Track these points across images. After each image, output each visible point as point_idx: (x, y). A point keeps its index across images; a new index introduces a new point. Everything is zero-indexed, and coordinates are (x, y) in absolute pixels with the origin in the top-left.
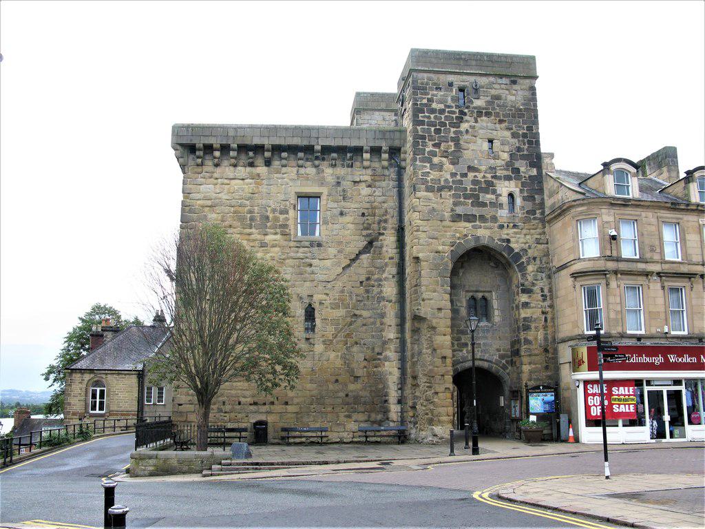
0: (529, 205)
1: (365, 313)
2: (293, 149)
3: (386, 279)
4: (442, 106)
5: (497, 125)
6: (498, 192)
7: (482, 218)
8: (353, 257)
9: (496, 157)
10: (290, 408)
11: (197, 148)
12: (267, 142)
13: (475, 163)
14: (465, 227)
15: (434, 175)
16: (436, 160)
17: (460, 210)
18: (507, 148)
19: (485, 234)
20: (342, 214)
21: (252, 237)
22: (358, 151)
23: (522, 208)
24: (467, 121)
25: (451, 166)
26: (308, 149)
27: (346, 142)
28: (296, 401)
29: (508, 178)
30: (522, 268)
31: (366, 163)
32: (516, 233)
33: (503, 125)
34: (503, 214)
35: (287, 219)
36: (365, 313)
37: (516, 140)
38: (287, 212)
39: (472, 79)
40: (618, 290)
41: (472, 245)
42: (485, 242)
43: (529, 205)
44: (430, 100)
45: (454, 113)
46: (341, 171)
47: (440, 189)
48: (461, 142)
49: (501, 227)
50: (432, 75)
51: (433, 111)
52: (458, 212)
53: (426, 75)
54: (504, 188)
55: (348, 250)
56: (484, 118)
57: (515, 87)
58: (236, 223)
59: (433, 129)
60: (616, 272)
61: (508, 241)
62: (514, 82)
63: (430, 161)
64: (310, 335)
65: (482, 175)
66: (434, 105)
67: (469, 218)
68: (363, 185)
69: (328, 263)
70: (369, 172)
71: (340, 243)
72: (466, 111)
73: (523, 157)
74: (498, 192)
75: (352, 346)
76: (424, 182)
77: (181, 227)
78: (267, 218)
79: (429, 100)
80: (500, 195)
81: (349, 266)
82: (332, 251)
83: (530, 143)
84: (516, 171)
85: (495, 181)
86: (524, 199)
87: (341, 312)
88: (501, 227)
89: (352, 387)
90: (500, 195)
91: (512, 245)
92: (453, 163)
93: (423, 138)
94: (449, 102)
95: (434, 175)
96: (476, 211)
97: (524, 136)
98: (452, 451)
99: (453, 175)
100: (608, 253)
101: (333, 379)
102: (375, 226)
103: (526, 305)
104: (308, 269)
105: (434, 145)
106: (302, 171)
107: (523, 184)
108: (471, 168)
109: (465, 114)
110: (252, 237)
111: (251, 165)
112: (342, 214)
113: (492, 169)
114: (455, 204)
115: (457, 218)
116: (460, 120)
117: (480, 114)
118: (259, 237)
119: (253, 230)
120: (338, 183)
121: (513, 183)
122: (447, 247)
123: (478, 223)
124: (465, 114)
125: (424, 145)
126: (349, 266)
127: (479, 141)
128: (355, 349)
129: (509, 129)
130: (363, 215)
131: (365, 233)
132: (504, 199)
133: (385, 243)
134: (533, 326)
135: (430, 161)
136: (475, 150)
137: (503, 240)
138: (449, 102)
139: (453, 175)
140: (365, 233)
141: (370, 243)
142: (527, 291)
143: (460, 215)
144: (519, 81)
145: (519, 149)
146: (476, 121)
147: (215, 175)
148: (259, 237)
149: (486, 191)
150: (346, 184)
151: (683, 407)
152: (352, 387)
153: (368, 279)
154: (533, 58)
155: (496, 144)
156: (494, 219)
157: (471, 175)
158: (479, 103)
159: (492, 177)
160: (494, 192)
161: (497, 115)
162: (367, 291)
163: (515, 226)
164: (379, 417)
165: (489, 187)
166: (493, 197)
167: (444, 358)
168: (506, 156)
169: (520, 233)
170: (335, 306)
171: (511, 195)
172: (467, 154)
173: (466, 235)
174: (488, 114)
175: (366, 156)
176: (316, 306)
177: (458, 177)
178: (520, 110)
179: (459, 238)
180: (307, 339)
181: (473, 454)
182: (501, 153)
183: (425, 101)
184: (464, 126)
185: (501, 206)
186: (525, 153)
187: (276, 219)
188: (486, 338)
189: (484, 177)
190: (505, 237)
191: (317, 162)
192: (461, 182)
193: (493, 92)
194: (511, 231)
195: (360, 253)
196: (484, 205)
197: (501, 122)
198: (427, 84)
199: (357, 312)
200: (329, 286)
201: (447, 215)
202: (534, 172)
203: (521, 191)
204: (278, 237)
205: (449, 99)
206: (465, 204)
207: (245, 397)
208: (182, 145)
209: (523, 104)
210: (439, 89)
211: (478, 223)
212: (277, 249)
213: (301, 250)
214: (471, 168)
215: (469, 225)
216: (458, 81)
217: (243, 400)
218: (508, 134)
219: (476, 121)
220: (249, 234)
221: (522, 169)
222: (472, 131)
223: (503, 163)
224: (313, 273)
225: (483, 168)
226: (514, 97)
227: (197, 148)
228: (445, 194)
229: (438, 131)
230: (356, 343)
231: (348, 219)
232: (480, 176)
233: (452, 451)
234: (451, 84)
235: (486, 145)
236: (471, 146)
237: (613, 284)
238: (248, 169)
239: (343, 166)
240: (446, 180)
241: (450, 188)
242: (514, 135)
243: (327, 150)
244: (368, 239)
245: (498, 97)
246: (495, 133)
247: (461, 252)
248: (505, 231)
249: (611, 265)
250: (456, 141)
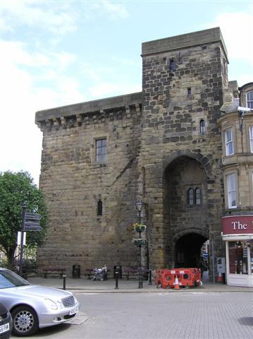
0: (214, 126)
1: (128, 203)
2: (90, 115)
3: (139, 182)
4: (159, 73)
5: (194, 78)
6: (193, 120)
7: (183, 138)
8: (122, 170)
9: (192, 98)
10: (90, 258)
11: (47, 120)
12: (77, 113)
13: (179, 105)
14: (171, 146)
15: (154, 116)
16: (155, 107)
17: (169, 135)
18: (199, 91)
19: (184, 148)
20: (116, 147)
21: (73, 165)
22: (123, 109)
23: (209, 128)
24: (174, 79)
25: (165, 109)
26: (97, 113)
27: (118, 106)
28: (92, 254)
29: (200, 110)
30: (209, 167)
31: (129, 116)
32: (204, 145)
33: (197, 77)
34: (196, 134)
35: (89, 153)
36: (128, 203)
37: (205, 85)
38: (89, 150)
39: (178, 52)
40: (247, 176)
41: (176, 156)
42: (184, 153)
43: (214, 126)
44: (152, 72)
45: (167, 76)
46: (116, 122)
47: (157, 124)
48: (170, 93)
49: (195, 142)
50: (154, 56)
51: (154, 78)
52: (168, 137)
53: (150, 57)
54: (196, 118)
55: (119, 167)
56: (185, 75)
57: (205, 51)
58: (65, 159)
59: (154, 88)
60: (244, 164)
61: (199, 150)
62: (205, 48)
63: (151, 108)
64: (100, 217)
65: (182, 111)
66: (155, 74)
67: (174, 139)
68: (128, 128)
69: (109, 176)
70: (131, 120)
71: (115, 163)
72: (174, 73)
73: (210, 95)
74: (193, 120)
75: (121, 222)
76: (148, 121)
77: (42, 164)
78: (80, 154)
79: (152, 72)
80: (194, 122)
81: (120, 176)
82: (111, 168)
83: (215, 85)
84: (205, 105)
85: (191, 114)
86: (210, 122)
87: (115, 203)
88: (195, 142)
89: (120, 246)
90: (194, 122)
91: (202, 153)
92: (165, 107)
93: (148, 95)
94: (164, 70)
95: (154, 116)
96: (178, 134)
97: (211, 81)
98: (117, 286)
99: (165, 114)
100: (240, 151)
101: (111, 241)
102: (133, 152)
103: (210, 191)
104: (99, 180)
105: (154, 98)
106: (97, 126)
107: (210, 113)
108: (176, 108)
109: (173, 75)
110: (73, 165)
111: (73, 126)
112: (116, 147)
113: (190, 106)
114: (166, 132)
115: (166, 140)
116: (170, 79)
117: (182, 73)
118: (76, 165)
119: (73, 162)
120: (115, 129)
121: (202, 113)
122: (160, 160)
123: (180, 142)
124: (173, 75)
125: (149, 99)
126: (120, 176)
127: (181, 90)
128: (122, 224)
129: (200, 79)
130: (128, 146)
131: (128, 156)
132: (197, 124)
133: (139, 160)
134: (215, 205)
135: (151, 108)
136: (179, 95)
137: (196, 151)
138: (164, 70)
139: (165, 114)
140: (128, 156)
141: (132, 161)
142: (212, 182)
143: (168, 138)
144: (208, 46)
145: (207, 90)
146: (180, 78)
147: (57, 135)
148: (76, 165)
149: (185, 121)
150: (119, 130)
151: (230, 261)
152: (120, 246)
153: (130, 183)
154: (218, 29)
155: (193, 90)
156: (190, 138)
157: (176, 113)
158: (181, 66)
159: (189, 111)
160: (190, 121)
161: (193, 71)
162: (129, 190)
163: (203, 140)
164: (135, 264)
165: (187, 118)
166: (190, 124)
167: (158, 228)
168: (198, 97)
169: (207, 145)
170: (112, 200)
171: (202, 121)
172: (174, 100)
173: (172, 151)
174: (187, 72)
175: (128, 111)
176: (103, 200)
177: (168, 115)
178: (209, 65)
179: (168, 153)
180: (98, 219)
181: (139, 287)
182: (195, 95)
183: (150, 73)
184: (173, 82)
185: (195, 129)
186: (212, 92)
187: (84, 154)
188: (197, 214)
189: (184, 112)
190: (197, 148)
191: (103, 120)
192: (169, 118)
193: (191, 58)
194: (201, 144)
195: (126, 168)
196: (184, 129)
197: (195, 75)
198: (151, 62)
199: (124, 203)
200: (109, 188)
201: (161, 139)
202: (218, 103)
203: (208, 117)
204: (85, 164)
205: (164, 68)
206: (172, 131)
207: (68, 252)
208: (40, 122)
209: (210, 61)
210: (158, 63)
211: (180, 142)
212: (84, 170)
213: (96, 170)
214: (176, 108)
215: (174, 144)
216: (168, 55)
217: (67, 254)
218: (200, 82)
219: (180, 78)
220: (72, 164)
221: (209, 103)
222: (178, 85)
223: (197, 101)
224: (101, 182)
225: (183, 107)
226: (206, 57)
227: (47, 120)
228: (160, 126)
229: (156, 89)
230: (123, 220)
231: (119, 149)
232: (181, 112)
233: (117, 286)
234: (165, 59)
235: (186, 92)
236: (177, 94)
237: (243, 172)
238: (72, 129)
239: (117, 119)
240: (161, 118)
241: (163, 123)
242: (204, 82)
243: (108, 111)
244: (130, 159)
245: (194, 60)
246: (192, 83)
247: (169, 161)
248: (197, 144)
249: (242, 159)
250: (167, 93)
